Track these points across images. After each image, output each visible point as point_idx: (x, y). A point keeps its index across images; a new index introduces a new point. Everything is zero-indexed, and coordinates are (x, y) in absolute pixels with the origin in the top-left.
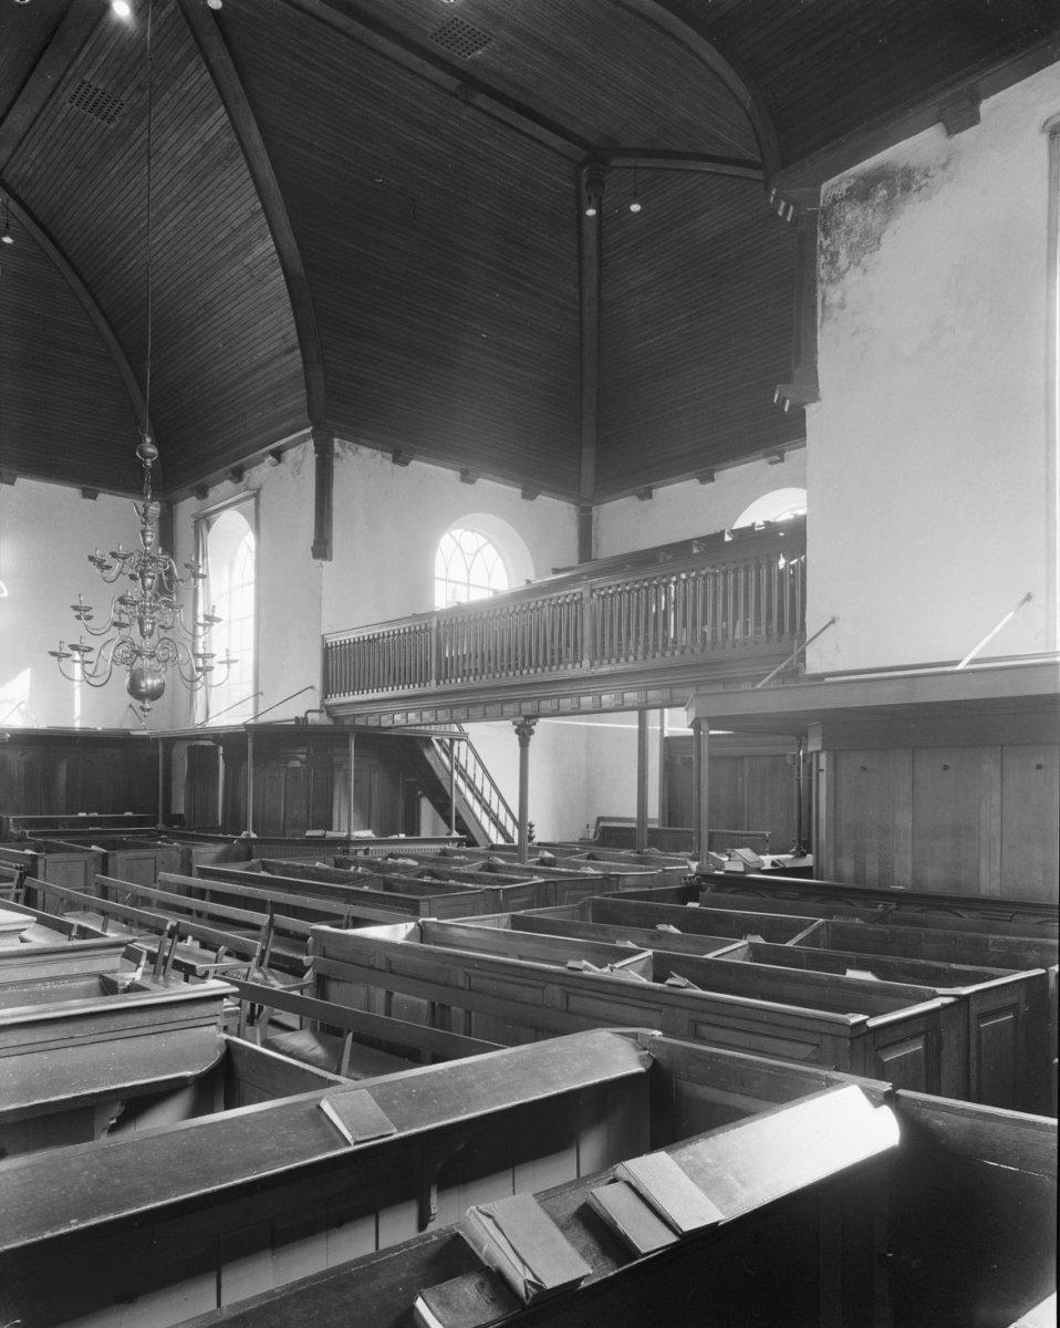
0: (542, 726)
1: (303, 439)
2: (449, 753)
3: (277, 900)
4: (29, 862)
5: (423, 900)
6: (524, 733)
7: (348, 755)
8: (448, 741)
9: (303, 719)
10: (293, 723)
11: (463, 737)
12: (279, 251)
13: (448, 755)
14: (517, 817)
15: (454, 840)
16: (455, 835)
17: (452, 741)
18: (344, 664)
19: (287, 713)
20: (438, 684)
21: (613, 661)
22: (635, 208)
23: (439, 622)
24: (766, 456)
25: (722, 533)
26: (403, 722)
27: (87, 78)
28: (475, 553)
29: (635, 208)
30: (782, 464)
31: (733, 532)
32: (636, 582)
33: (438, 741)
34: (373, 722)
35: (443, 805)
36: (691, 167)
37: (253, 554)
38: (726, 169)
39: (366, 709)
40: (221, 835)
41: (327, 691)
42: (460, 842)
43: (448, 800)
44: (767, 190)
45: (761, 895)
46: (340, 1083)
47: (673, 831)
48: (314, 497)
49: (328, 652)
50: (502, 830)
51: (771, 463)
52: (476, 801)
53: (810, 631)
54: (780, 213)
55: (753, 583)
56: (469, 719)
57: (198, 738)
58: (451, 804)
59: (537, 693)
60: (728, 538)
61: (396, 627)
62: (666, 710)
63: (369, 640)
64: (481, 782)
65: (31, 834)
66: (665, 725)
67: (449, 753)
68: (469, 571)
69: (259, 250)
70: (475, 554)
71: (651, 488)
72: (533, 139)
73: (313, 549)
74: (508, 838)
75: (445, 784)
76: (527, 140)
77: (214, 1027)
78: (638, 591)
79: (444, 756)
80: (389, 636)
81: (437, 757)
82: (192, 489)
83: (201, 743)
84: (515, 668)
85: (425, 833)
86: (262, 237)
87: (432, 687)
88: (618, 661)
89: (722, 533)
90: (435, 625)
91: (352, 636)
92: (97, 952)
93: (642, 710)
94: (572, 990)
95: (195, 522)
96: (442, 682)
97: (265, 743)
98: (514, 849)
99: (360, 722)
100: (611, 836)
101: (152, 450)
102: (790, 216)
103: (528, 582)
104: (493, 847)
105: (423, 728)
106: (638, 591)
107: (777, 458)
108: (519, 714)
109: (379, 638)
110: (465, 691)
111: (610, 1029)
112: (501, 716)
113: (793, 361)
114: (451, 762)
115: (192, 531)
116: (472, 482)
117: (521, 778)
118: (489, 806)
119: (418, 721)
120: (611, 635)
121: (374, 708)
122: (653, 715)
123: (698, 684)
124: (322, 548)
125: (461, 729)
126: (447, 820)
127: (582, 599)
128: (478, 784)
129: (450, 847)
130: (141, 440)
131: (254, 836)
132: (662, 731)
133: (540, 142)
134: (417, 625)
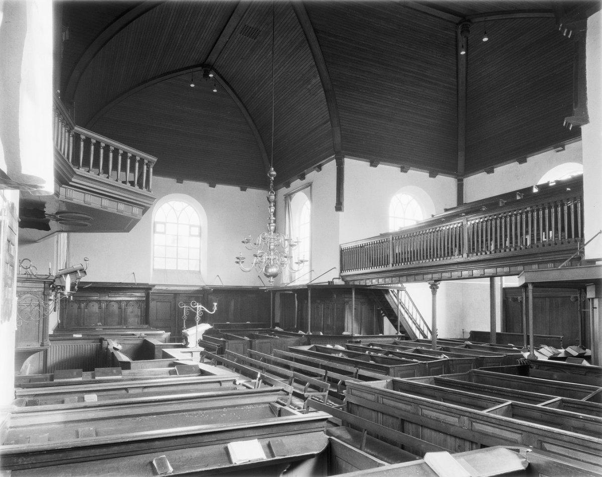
0: (442, 285)
1: (332, 160)
2: (397, 297)
3: (323, 364)
4: (222, 344)
5: (392, 368)
6: (434, 288)
7: (352, 298)
8: (396, 291)
9: (332, 282)
10: (327, 284)
11: (403, 289)
12: (322, 81)
13: (396, 297)
14: (431, 329)
15: (399, 336)
16: (400, 334)
17: (398, 291)
18: (348, 257)
19: (324, 280)
20: (393, 266)
21: (479, 254)
22: (485, 39)
23: (393, 238)
24: (555, 148)
25: (531, 188)
26: (377, 283)
27: (247, 24)
28: (402, 200)
29: (485, 39)
30: (564, 151)
31: (538, 187)
32: (490, 216)
33: (391, 291)
34: (362, 283)
35: (394, 319)
36: (513, 17)
37: (310, 211)
38: (531, 15)
39: (359, 277)
40: (292, 332)
41: (342, 270)
42: (402, 338)
43: (396, 318)
44: (558, 23)
45: (564, 372)
46: (384, 465)
47: (508, 334)
48: (336, 187)
49: (342, 251)
50: (422, 333)
51: (558, 151)
52: (409, 318)
53: (587, 238)
54: (565, 34)
55: (553, 215)
56: (407, 281)
57: (286, 290)
58: (398, 320)
59: (440, 269)
60: (535, 190)
61: (377, 240)
62: (504, 277)
63: (361, 247)
64: (412, 310)
65: (221, 331)
66: (503, 282)
67: (397, 297)
68: (178, 219)
69: (314, 81)
70: (182, 210)
71: (493, 168)
72: (436, 16)
73: (336, 207)
74: (425, 336)
75: (395, 311)
76: (432, 18)
77: (322, 432)
78: (491, 220)
79: (394, 298)
80: (370, 245)
81: (391, 298)
82: (284, 184)
83: (288, 292)
84: (422, 256)
85: (386, 333)
86: (315, 76)
87: (390, 267)
88: (481, 254)
89: (531, 188)
90: (391, 239)
91: (353, 245)
92: (268, 394)
93: (492, 278)
94: (474, 420)
95: (285, 198)
96: (394, 265)
97: (321, 293)
98: (429, 342)
99: (357, 283)
100: (477, 336)
101: (274, 173)
102: (570, 35)
103: (433, 216)
104: (418, 341)
105: (385, 285)
106: (491, 220)
107: (561, 148)
108: (432, 279)
109: (365, 246)
110: (406, 269)
111: (507, 447)
112: (423, 280)
113: (574, 104)
114: (398, 300)
115: (284, 202)
116: (182, 183)
117: (432, 309)
118: (419, 326)
119: (383, 283)
120: (478, 241)
121: (363, 277)
122: (497, 280)
123: (524, 265)
124: (339, 207)
125: (402, 286)
126: (396, 327)
127: (462, 225)
128: (410, 311)
129: (397, 339)
130: (269, 169)
131: (311, 334)
132: (501, 285)
133: (439, 18)
134: (383, 239)
